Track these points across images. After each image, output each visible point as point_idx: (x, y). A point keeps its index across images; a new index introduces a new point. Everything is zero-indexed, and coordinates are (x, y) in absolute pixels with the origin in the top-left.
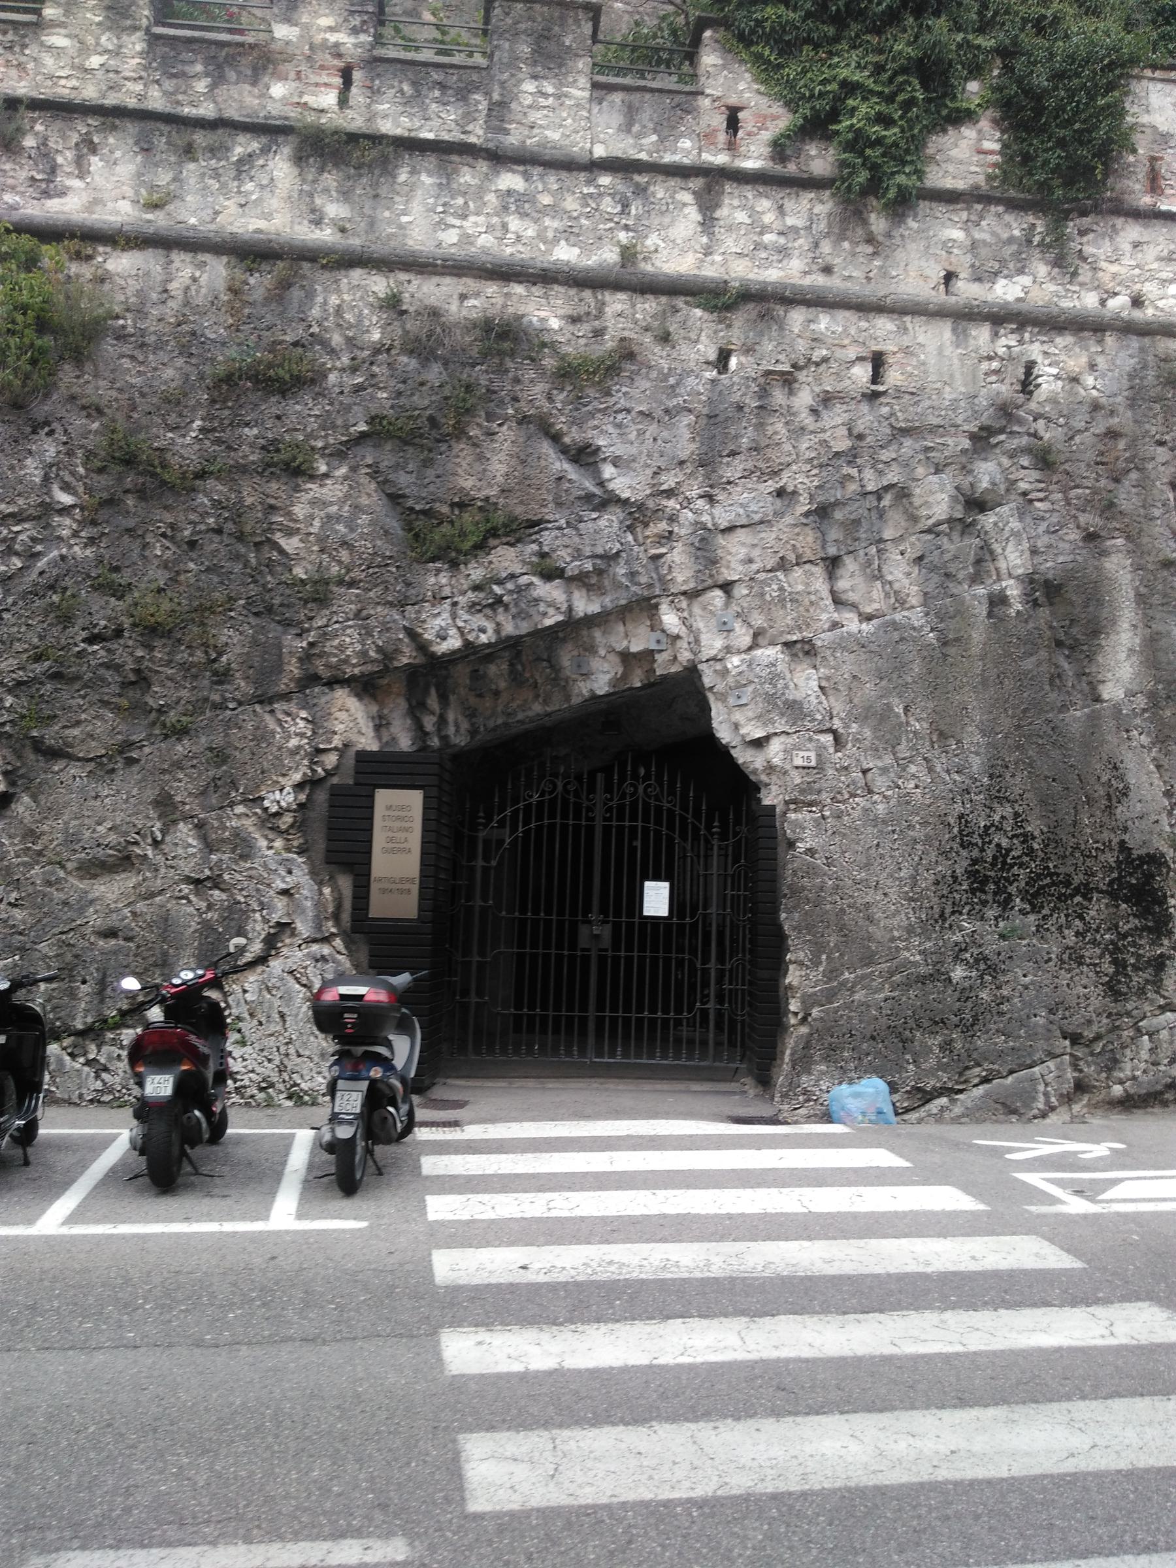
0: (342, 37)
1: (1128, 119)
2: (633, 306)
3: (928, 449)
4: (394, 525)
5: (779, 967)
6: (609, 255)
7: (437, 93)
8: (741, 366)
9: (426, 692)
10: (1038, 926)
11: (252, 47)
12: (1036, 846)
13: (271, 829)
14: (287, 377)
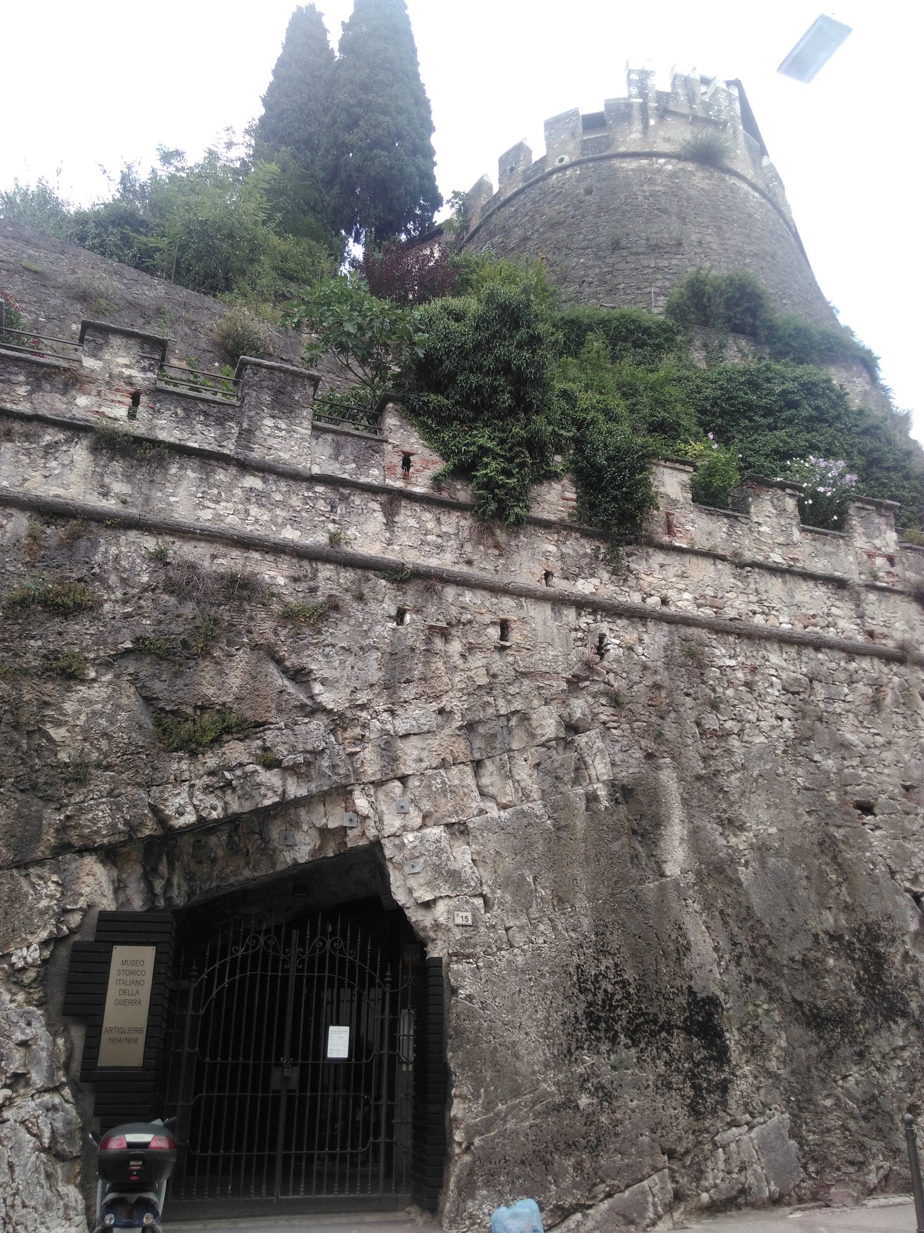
0: (134, 372)
1: (653, 489)
2: (338, 574)
3: (539, 688)
4: (147, 721)
5: (445, 1101)
6: (320, 538)
7: (202, 418)
8: (413, 621)
9: (159, 859)
10: (638, 1058)
11: (65, 370)
12: (632, 991)
13: (15, 983)
14: (71, 604)
